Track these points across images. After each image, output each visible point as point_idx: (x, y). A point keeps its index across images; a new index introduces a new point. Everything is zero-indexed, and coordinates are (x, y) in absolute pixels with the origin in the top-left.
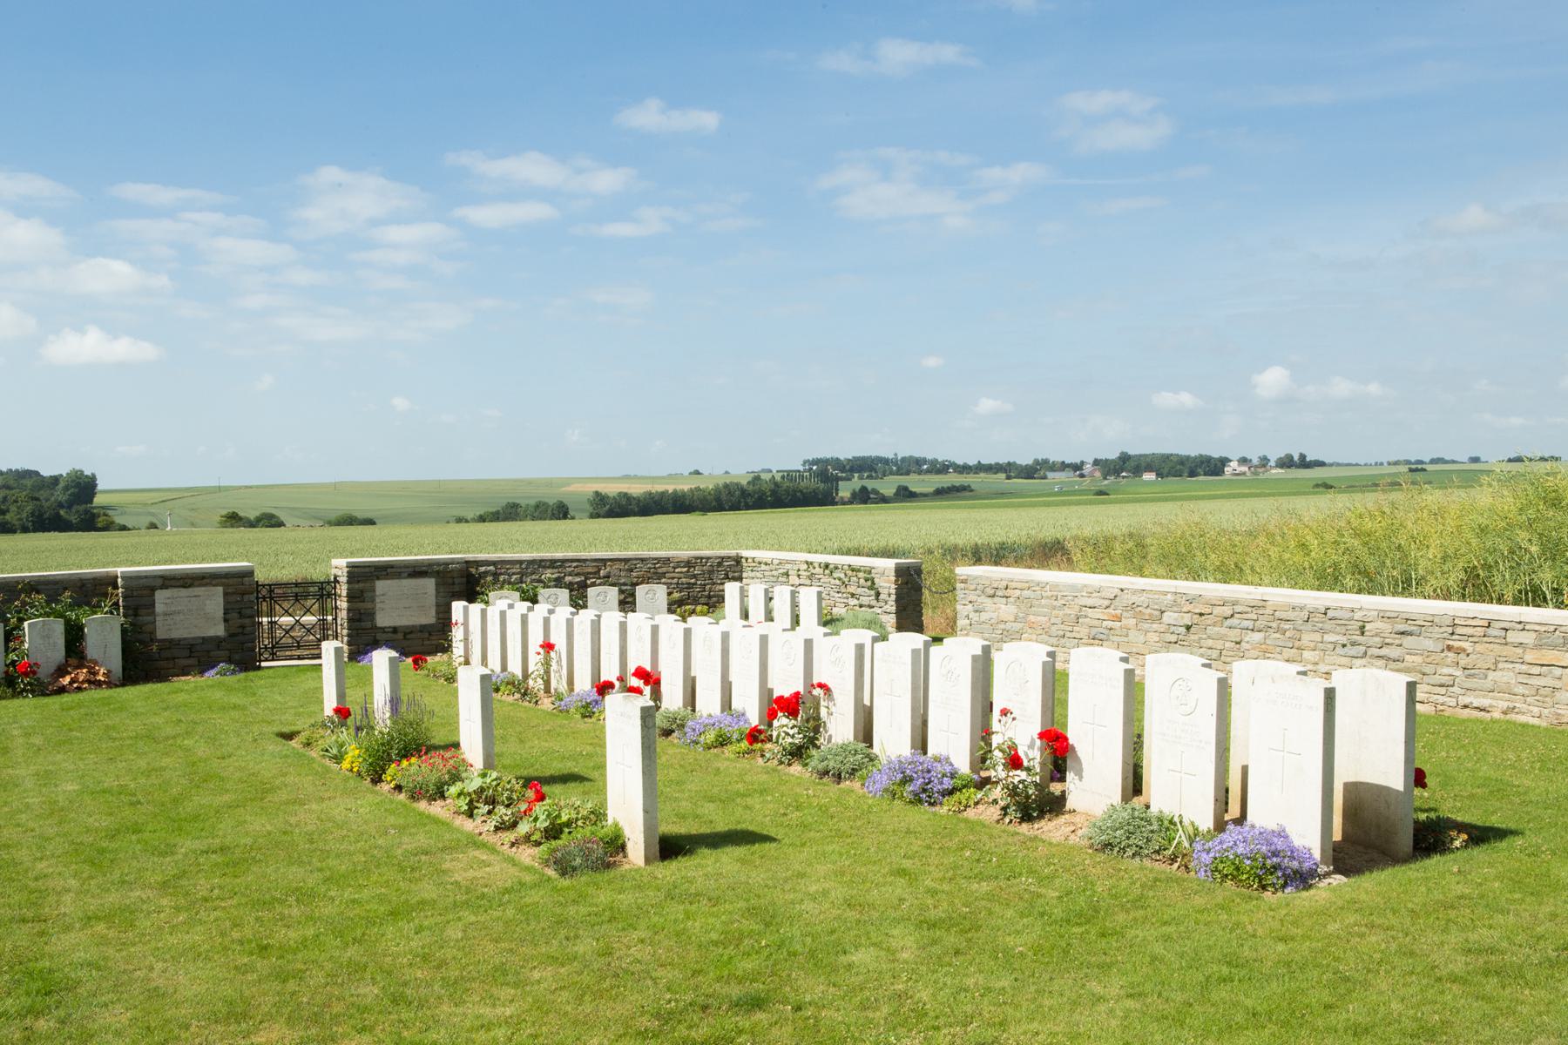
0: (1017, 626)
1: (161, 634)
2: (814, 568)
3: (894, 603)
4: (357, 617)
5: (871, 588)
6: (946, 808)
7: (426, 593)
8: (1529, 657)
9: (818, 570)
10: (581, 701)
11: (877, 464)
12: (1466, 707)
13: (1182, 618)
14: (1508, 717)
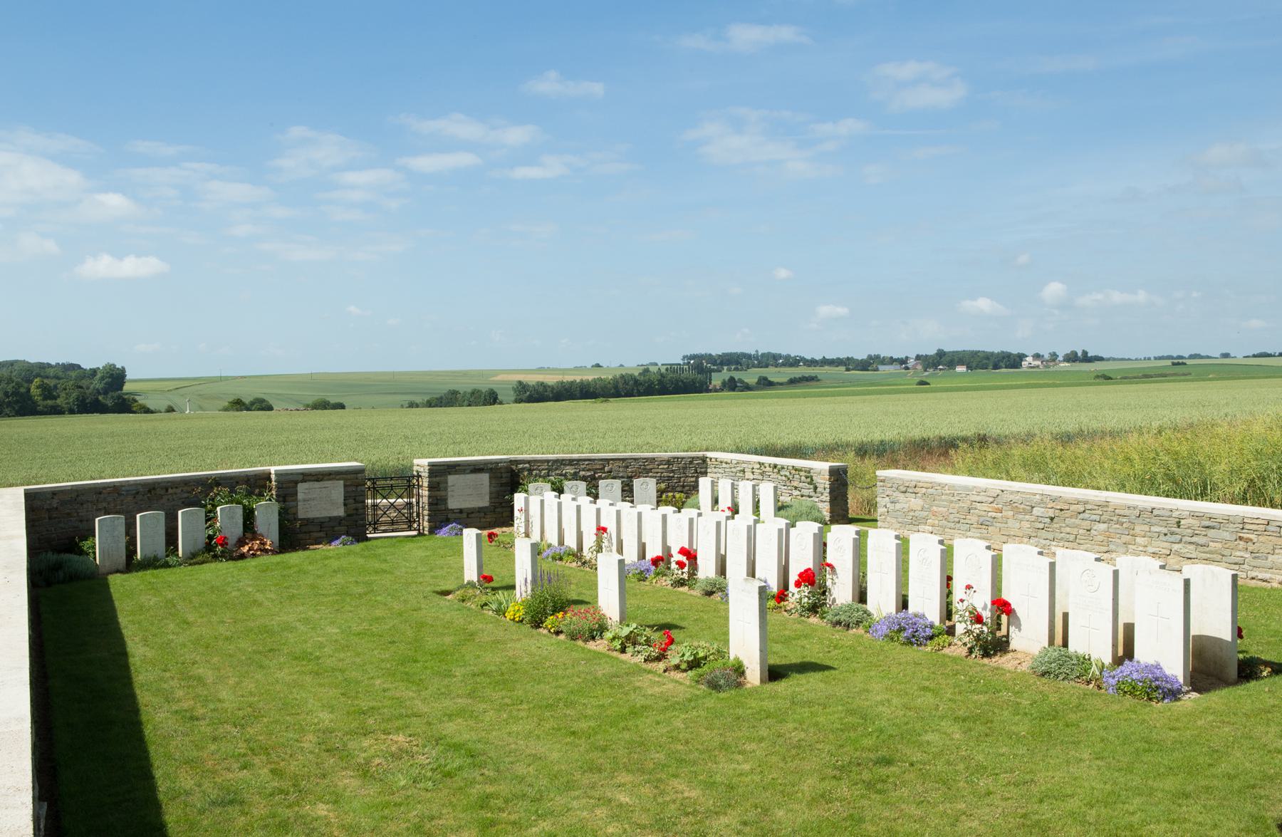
1: (301, 515)
2: (765, 467)
3: (828, 495)
4: (435, 502)
5: (810, 483)
7: (482, 484)
9: (768, 469)
10: (636, 569)
11: (742, 359)
12: (1253, 578)
13: (1048, 512)
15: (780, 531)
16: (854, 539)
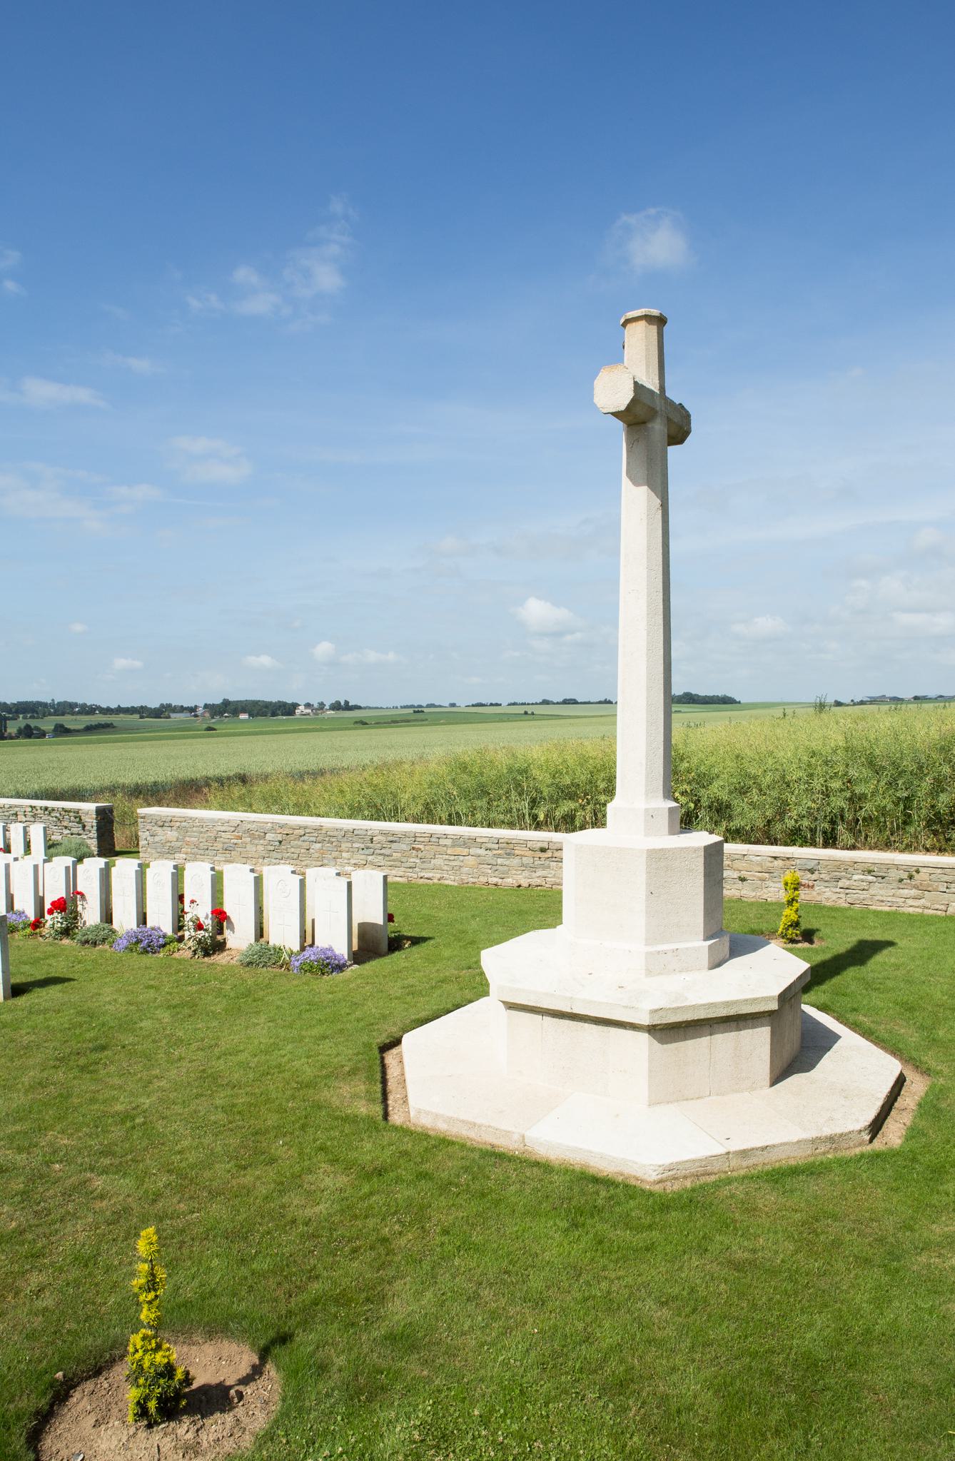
0: (179, 844)
2: (37, 810)
3: (95, 832)
6: (162, 954)
8: (449, 852)
9: (39, 811)
11: (38, 708)
12: (421, 878)
14: (440, 882)
15: (67, 868)
16: (136, 871)
